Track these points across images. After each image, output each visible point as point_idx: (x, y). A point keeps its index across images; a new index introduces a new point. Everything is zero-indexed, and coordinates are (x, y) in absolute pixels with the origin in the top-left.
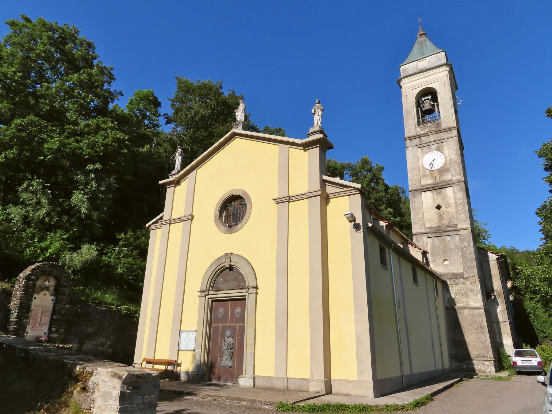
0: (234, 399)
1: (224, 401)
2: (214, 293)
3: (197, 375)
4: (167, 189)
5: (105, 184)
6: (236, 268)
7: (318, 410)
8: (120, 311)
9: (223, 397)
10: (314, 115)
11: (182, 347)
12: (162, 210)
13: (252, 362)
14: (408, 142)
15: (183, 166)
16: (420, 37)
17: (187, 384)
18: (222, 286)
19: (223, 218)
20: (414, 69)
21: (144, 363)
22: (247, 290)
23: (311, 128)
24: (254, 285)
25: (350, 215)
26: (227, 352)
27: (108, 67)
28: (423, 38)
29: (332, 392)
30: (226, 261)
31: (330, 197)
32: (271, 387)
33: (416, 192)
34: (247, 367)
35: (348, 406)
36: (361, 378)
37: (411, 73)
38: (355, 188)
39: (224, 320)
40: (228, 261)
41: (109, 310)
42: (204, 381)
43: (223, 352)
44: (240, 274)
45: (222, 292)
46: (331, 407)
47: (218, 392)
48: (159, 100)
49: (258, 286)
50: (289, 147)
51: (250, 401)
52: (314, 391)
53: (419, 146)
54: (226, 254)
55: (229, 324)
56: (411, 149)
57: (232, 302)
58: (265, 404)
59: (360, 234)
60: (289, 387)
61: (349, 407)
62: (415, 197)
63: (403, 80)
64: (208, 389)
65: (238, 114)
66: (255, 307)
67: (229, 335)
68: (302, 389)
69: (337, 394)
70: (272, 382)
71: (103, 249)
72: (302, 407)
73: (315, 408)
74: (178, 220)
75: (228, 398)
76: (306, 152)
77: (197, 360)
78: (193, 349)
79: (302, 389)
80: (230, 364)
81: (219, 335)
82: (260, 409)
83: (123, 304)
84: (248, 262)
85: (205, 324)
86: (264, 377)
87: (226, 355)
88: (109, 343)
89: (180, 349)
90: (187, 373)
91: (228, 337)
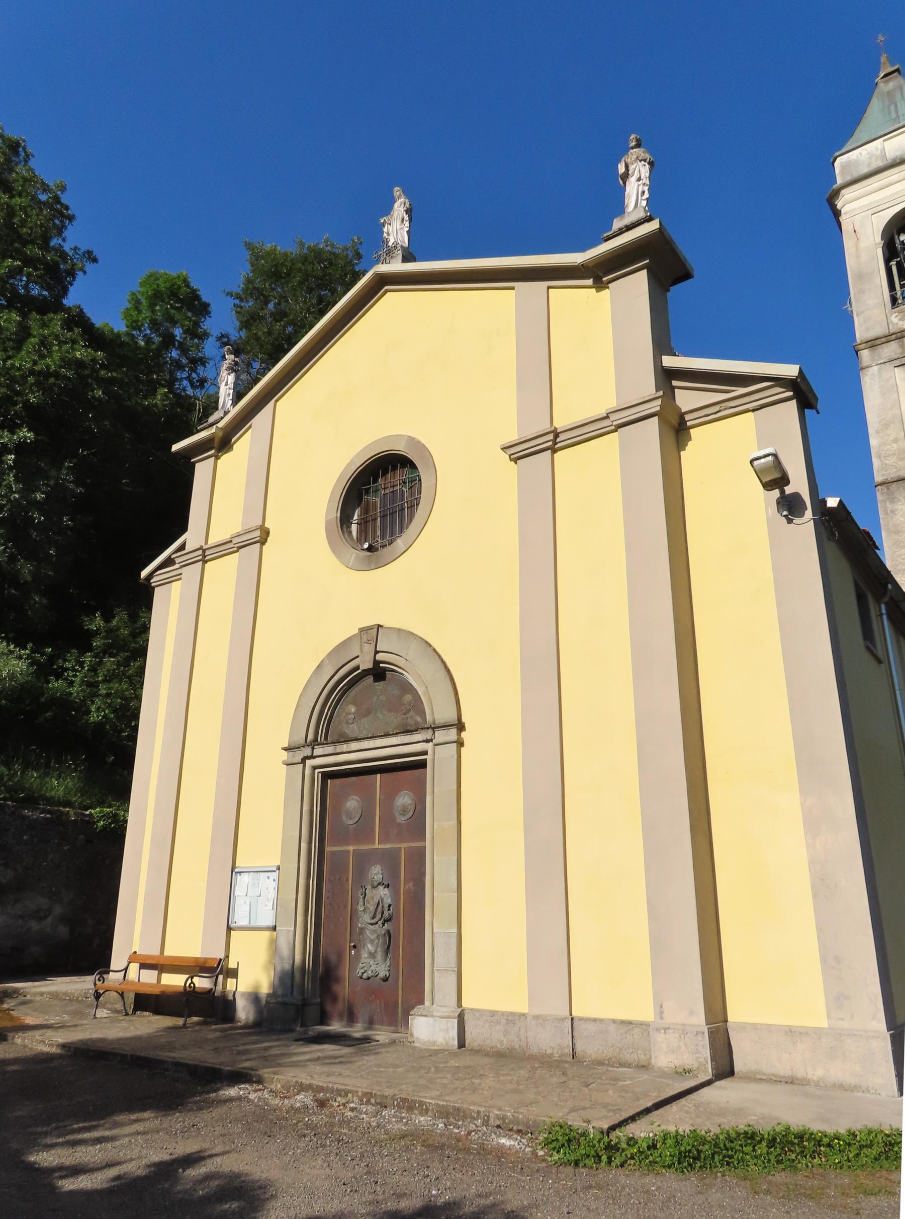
0: (389, 1101)
1: (352, 1109)
2: (329, 749)
3: (284, 1004)
4: (197, 465)
5: (47, 485)
6: (393, 671)
7: (713, 1158)
8: (90, 822)
9: (350, 1095)
10: (625, 183)
11: (240, 917)
12: (183, 527)
13: (453, 964)
14: (865, 354)
15: (238, 396)
17: (249, 1034)
18: (352, 730)
19: (354, 528)
20: (873, 160)
21: (134, 967)
22: (428, 735)
23: (615, 220)
24: (452, 717)
25: (770, 458)
26: (375, 931)
27: (52, 185)
29: (736, 1069)
30: (362, 652)
31: (689, 424)
32: (517, 1047)
33: (894, 485)
34: (436, 980)
35: (825, 1141)
36: (843, 1019)
37: (865, 170)
38: (777, 381)
39: (363, 831)
40: (369, 649)
41: (59, 820)
42: (302, 1026)
43: (362, 930)
44: (407, 688)
45: (354, 746)
46: (760, 1142)
47: (337, 1069)
48: (205, 299)
49: (464, 720)
50: (549, 288)
51: (445, 1113)
53: (897, 363)
54: (361, 630)
55: (377, 845)
56: (876, 373)
58: (503, 1127)
59: (806, 525)
60: (579, 1048)
61: (829, 1145)
62: (893, 499)
63: (843, 192)
64: (307, 1057)
65: (390, 228)
66: (455, 787)
67: (378, 878)
68: (628, 1057)
69: (753, 1078)
70: (522, 1031)
71: (52, 659)
72: (645, 1145)
73: (699, 1152)
74: (228, 548)
75: (367, 1097)
76: (606, 293)
77: (281, 958)
78: (271, 923)
79: (628, 1057)
80: (383, 972)
81: (347, 880)
82: (484, 1151)
83: (101, 803)
84: (430, 650)
85: (304, 845)
86: (493, 1013)
87: (372, 942)
88: (58, 910)
89: (232, 925)
90: (255, 998)
91: (376, 884)
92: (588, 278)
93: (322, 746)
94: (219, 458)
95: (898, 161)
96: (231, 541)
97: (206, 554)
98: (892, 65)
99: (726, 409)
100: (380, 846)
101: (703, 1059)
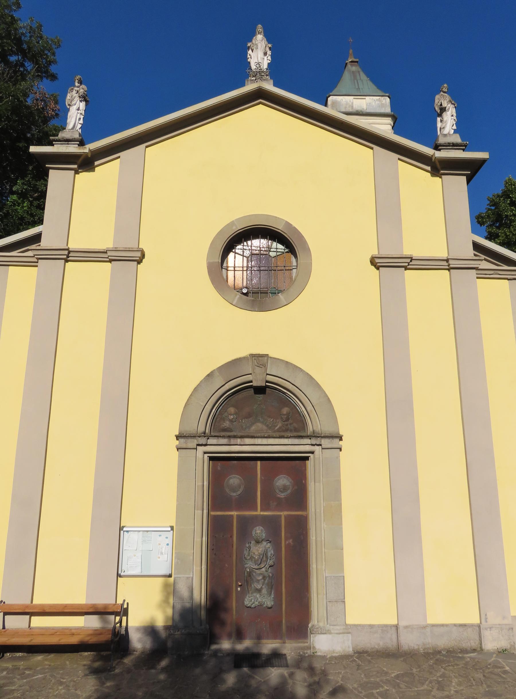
16: (351, 65)
28: (354, 68)
31: (223, 268)
45: (247, 441)
52: (496, 648)
57: (264, 462)
77: (181, 599)
86: (371, 626)
89: (122, 574)
92: (428, 165)
93: (216, 438)
94: (78, 174)
95: (361, 113)
96: (106, 252)
97: (70, 255)
98: (355, 58)
99: (495, 274)
100: (262, 513)
101: (513, 643)
